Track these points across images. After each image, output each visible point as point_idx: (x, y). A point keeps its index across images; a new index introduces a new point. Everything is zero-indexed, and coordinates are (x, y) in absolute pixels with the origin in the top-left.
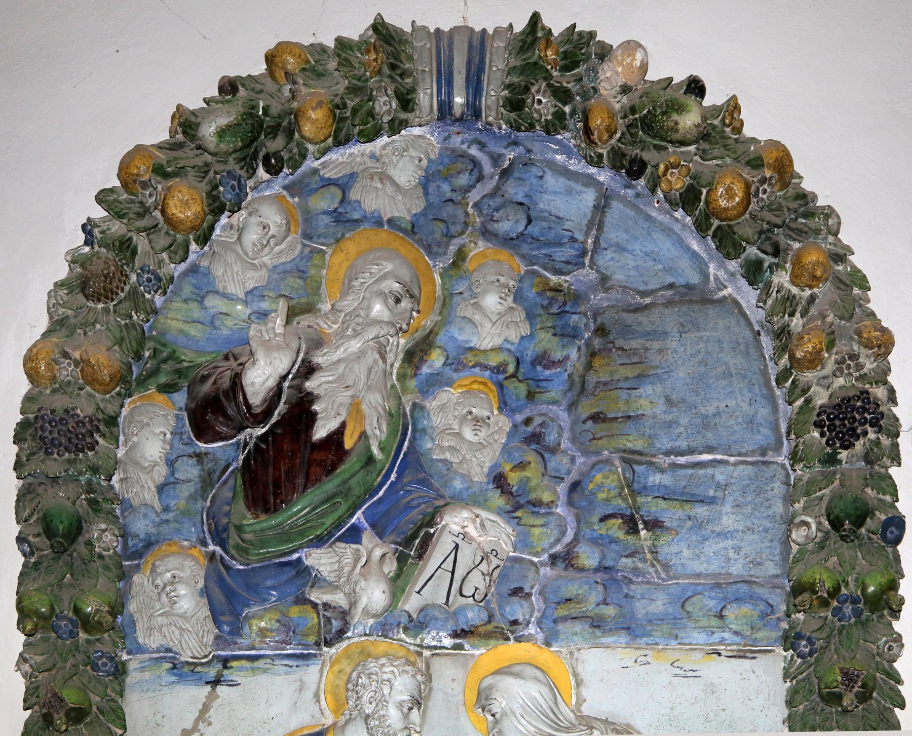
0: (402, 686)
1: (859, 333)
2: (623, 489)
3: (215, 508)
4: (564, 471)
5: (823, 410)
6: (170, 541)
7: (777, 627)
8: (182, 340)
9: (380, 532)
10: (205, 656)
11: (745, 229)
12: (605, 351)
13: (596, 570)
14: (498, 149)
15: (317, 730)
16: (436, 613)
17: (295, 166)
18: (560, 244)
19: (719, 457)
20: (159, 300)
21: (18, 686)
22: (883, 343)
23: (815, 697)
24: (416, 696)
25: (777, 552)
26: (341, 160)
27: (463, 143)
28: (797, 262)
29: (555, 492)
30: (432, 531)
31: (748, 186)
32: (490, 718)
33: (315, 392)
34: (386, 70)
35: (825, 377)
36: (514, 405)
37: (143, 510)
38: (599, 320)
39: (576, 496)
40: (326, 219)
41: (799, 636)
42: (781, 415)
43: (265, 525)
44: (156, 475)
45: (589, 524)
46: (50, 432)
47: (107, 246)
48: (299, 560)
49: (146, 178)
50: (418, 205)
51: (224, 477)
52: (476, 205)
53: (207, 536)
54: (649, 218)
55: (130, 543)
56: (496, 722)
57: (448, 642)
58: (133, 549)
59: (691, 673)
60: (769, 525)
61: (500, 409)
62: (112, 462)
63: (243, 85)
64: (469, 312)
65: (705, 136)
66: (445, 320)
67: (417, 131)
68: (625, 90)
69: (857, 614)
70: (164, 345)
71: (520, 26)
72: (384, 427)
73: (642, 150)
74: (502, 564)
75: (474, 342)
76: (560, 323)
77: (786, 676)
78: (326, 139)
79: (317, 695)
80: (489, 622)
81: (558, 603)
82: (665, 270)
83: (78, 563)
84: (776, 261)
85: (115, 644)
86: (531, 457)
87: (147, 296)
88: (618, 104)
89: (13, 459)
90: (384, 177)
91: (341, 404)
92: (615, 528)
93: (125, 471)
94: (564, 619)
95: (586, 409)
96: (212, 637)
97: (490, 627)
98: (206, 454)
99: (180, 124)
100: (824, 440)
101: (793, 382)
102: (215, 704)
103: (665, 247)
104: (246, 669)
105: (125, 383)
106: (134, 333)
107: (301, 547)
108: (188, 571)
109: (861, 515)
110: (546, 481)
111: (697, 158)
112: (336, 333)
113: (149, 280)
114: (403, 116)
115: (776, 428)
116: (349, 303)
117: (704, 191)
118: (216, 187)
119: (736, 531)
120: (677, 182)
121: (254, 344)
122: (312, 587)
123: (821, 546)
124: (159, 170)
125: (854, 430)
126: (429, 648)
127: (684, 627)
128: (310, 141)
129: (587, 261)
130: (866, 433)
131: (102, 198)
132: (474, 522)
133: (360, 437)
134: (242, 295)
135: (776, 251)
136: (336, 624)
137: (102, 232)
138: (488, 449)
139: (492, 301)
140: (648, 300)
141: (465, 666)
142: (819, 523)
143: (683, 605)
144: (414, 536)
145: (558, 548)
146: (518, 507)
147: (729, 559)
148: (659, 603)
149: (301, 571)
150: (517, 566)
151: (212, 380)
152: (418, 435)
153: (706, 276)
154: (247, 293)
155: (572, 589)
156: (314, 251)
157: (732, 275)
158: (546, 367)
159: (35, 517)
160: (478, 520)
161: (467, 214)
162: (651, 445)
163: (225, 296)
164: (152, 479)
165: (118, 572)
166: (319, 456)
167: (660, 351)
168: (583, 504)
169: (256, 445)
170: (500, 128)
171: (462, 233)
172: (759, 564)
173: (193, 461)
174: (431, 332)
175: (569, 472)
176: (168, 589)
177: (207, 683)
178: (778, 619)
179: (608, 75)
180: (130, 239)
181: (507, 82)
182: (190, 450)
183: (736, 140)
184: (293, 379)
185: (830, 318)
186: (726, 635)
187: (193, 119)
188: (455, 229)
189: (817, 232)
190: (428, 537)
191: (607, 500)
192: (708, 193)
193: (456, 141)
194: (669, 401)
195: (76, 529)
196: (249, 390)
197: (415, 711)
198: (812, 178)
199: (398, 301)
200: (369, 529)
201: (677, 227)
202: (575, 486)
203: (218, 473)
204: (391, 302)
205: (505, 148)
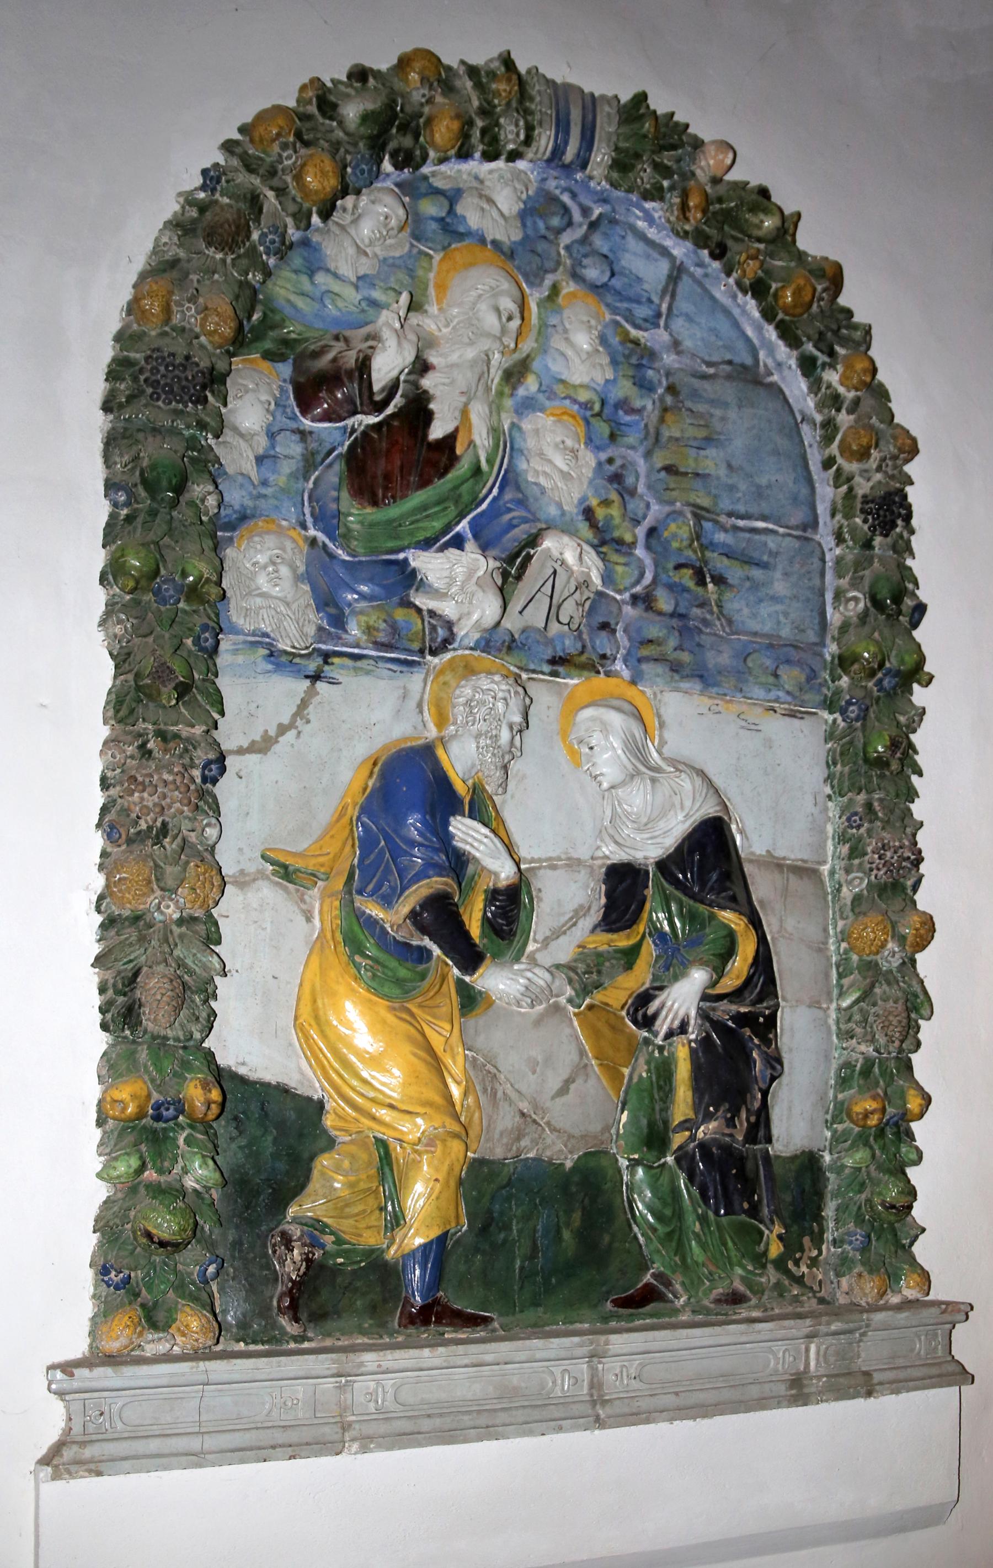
2: (693, 541)
3: (319, 491)
4: (640, 514)
7: (819, 691)
8: (288, 311)
10: (307, 648)
12: (676, 409)
13: (672, 615)
14: (587, 202)
18: (639, 302)
19: (771, 526)
25: (816, 621)
30: (532, 552)
33: (431, 392)
35: (866, 471)
38: (671, 379)
39: (654, 542)
40: (434, 226)
45: (665, 570)
46: (163, 376)
48: (406, 560)
50: (516, 235)
51: (328, 461)
52: (567, 248)
53: (309, 521)
58: (226, 520)
59: (753, 727)
60: (811, 596)
61: (585, 443)
63: (375, 78)
64: (563, 346)
66: (543, 348)
71: (625, 97)
79: (420, 706)
81: (642, 643)
82: (724, 347)
86: (614, 496)
97: (583, 658)
98: (311, 433)
102: (315, 700)
104: (348, 668)
105: (240, 341)
107: (408, 547)
113: (273, 242)
122: (417, 590)
128: (436, 149)
129: (662, 323)
131: (228, 146)
136: (441, 633)
140: (711, 371)
141: (560, 694)
143: (745, 660)
144: (517, 555)
145: (638, 589)
146: (603, 543)
147: (779, 623)
148: (726, 655)
154: (359, 278)
155: (654, 631)
156: (421, 252)
158: (626, 413)
161: (559, 254)
162: (716, 504)
163: (336, 276)
167: (723, 419)
169: (364, 433)
173: (296, 437)
174: (528, 356)
175: (645, 517)
177: (307, 677)
182: (294, 425)
190: (529, 558)
191: (680, 549)
193: (551, 185)
194: (730, 466)
196: (375, 376)
199: (510, 318)
200: (472, 541)
201: (736, 312)
203: (322, 455)
205: (595, 202)
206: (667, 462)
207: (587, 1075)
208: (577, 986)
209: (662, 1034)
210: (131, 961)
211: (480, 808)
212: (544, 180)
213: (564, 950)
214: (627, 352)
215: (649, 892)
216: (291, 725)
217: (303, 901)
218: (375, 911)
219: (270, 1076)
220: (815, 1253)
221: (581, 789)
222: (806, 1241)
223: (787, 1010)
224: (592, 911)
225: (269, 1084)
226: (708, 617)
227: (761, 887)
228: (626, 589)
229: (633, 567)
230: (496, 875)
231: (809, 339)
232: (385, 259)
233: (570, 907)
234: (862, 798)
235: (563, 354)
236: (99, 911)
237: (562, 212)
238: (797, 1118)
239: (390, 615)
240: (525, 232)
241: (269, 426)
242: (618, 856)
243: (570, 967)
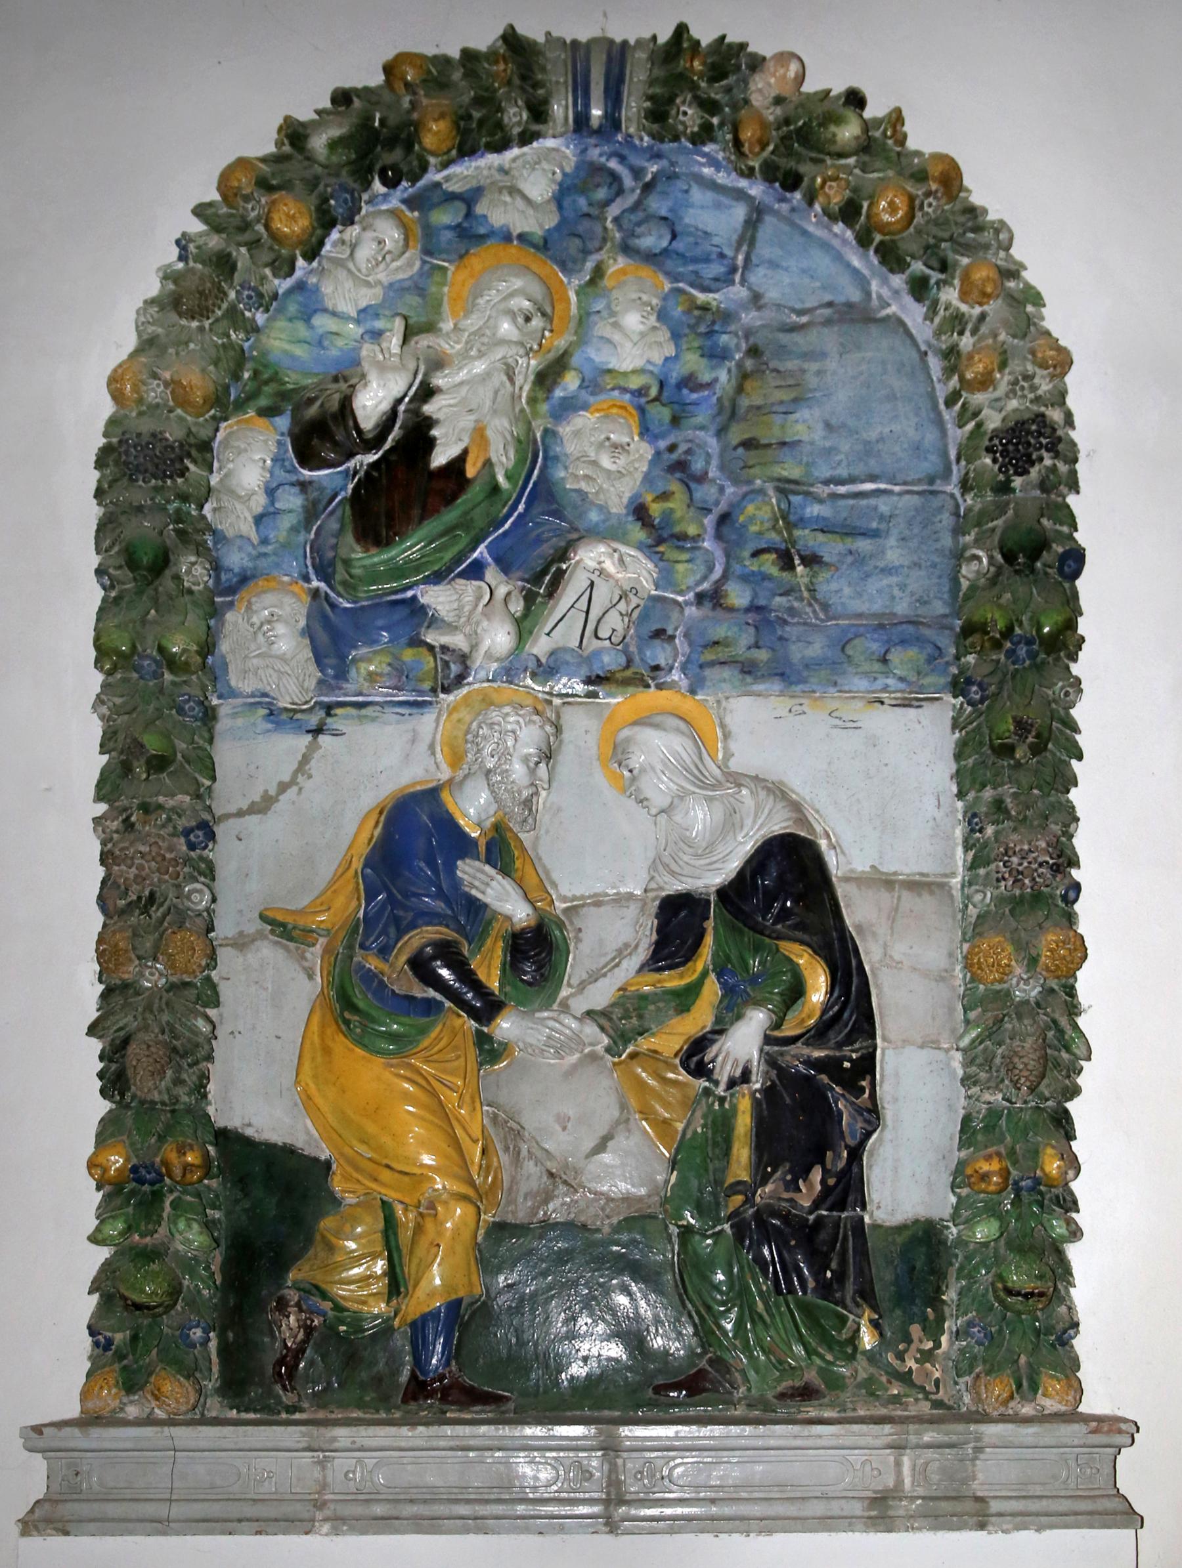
0: (529, 738)
1: (1033, 352)
5: (995, 434)
6: (267, 576)
9: (505, 566)
10: (306, 703)
11: (909, 243)
12: (758, 372)
13: (749, 609)
15: (430, 785)
16: (568, 657)
17: (414, 180)
18: (707, 260)
19: (883, 486)
20: (260, 318)
21: (95, 729)
22: (1062, 362)
23: (986, 749)
24: (544, 749)
25: (946, 589)
26: (463, 173)
27: (601, 155)
28: (966, 277)
29: (702, 525)
31: (911, 199)
32: (626, 773)
34: (517, 81)
35: (997, 400)
36: (657, 431)
37: (238, 542)
39: (725, 530)
40: (448, 235)
41: (969, 682)
42: (950, 440)
43: (376, 560)
44: (253, 503)
45: (740, 561)
47: (203, 262)
48: (414, 598)
49: (247, 191)
52: (616, 220)
53: (311, 570)
54: (805, 233)
55: (223, 577)
56: (634, 779)
57: (580, 688)
60: (937, 560)
61: (641, 435)
62: (204, 490)
63: (358, 97)
65: (867, 147)
67: (550, 143)
68: (779, 101)
69: (1032, 655)
70: (266, 366)
71: (664, 36)
72: (512, 455)
73: (798, 162)
74: (642, 603)
75: (613, 364)
76: (708, 343)
77: (955, 725)
78: (449, 151)
79: (432, 747)
80: (628, 667)
81: (705, 647)
83: (163, 599)
84: (943, 276)
85: (204, 689)
86: (675, 487)
87: (248, 314)
88: (772, 114)
89: (93, 486)
90: (514, 191)
91: (463, 430)
92: (769, 564)
93: (218, 500)
94: (712, 664)
95: (736, 434)
96: (314, 682)
97: (628, 673)
98: (311, 483)
99: (287, 136)
100: (997, 467)
101: (964, 405)
102: (317, 755)
103: (822, 262)
104: (352, 717)
105: (222, 404)
106: (232, 353)
107: (416, 584)
108: (288, 609)
109: (1038, 546)
110: (692, 512)
111: (857, 171)
112: (459, 354)
113: (249, 297)
114: (535, 127)
115: (945, 454)
116: (472, 323)
117: (865, 205)
118: (326, 201)
119: (902, 566)
120: (836, 196)
121: (366, 365)
123: (993, 581)
124: (264, 185)
125: (1029, 456)
126: (560, 695)
127: (844, 673)
128: (434, 154)
129: (737, 278)
130: (1041, 459)
131: (200, 211)
132: (611, 556)
133: (484, 465)
134: (354, 314)
135: (944, 267)
136: (455, 669)
137: (198, 247)
138: (627, 479)
139: (633, 321)
140: (804, 319)
142: (991, 558)
144: (544, 572)
145: (705, 586)
146: (660, 541)
147: (893, 598)
149: (417, 611)
150: (659, 605)
151: (318, 403)
152: (549, 463)
153: (868, 294)
155: (721, 631)
157: (896, 292)
158: (692, 390)
159: (116, 549)
160: (616, 555)
161: (605, 229)
163: (334, 314)
164: (249, 509)
165: (208, 609)
166: (437, 485)
167: (819, 373)
168: (734, 537)
169: (367, 473)
170: (641, 139)
171: (600, 249)
172: (926, 603)
173: (296, 490)
175: (717, 503)
176: (265, 628)
177: (308, 732)
178: (947, 663)
179: (760, 86)
180: (229, 255)
181: (650, 92)
182: (294, 478)
183: (899, 154)
184: (411, 401)
185: (1002, 336)
186: (891, 681)
187: (301, 130)
188: (591, 245)
189: (987, 247)
190: (561, 573)
191: (760, 533)
192: (870, 206)
193: (594, 154)
194: (828, 426)
195: (162, 563)
196: (359, 414)
197: (542, 765)
198: (984, 190)
199: (528, 319)
201: (836, 243)
202: (724, 519)
203: (324, 502)
204: (520, 320)
206: (746, 436)
207: (629, 1131)
208: (611, 1032)
209: (722, 1086)
210: (121, 1029)
211: (500, 850)
212: (584, 151)
213: (601, 995)
214: (693, 321)
215: (710, 925)
216: (293, 782)
217: (304, 958)
218: (373, 963)
219: (276, 1137)
220: (930, 1345)
221: (618, 819)
222: (915, 1330)
223: (890, 1053)
224: (640, 950)
225: (275, 1146)
226: (796, 604)
227: (858, 911)
228: (689, 588)
229: (698, 562)
230: (508, 918)
231: (913, 257)
232: (391, 285)
233: (612, 945)
234: (988, 794)
235: (609, 341)
236: (100, 981)
237: (609, 180)
238: (908, 1173)
239: (397, 658)
240: (562, 215)
241: (267, 484)
242: (676, 886)
243: (604, 1014)
